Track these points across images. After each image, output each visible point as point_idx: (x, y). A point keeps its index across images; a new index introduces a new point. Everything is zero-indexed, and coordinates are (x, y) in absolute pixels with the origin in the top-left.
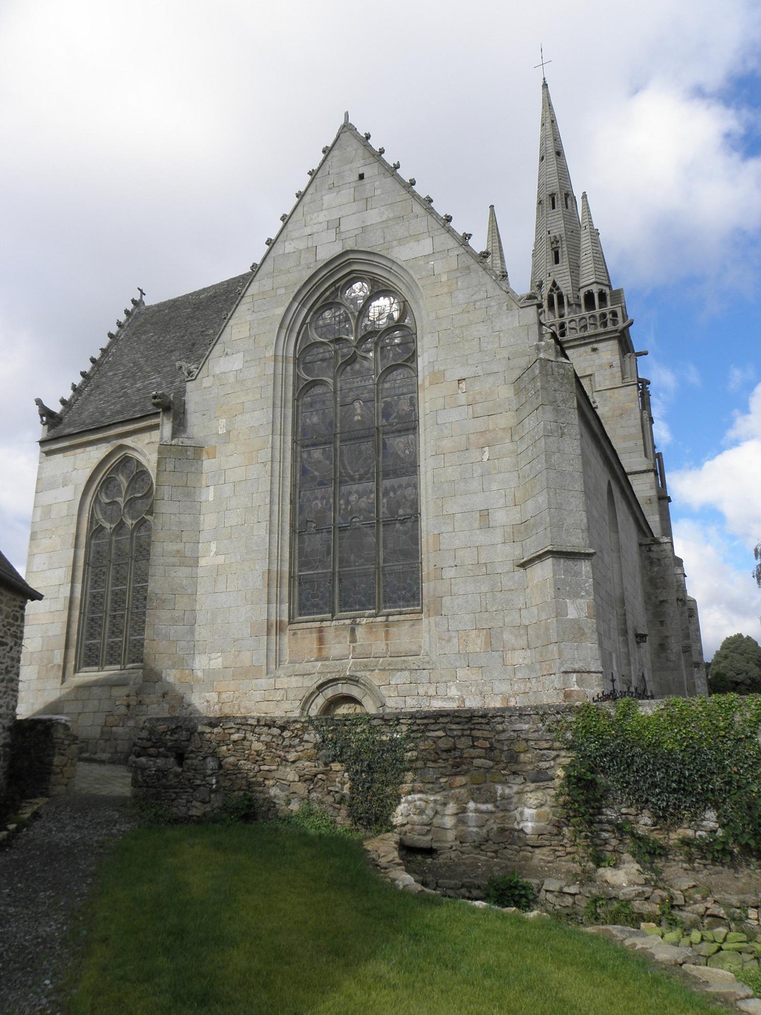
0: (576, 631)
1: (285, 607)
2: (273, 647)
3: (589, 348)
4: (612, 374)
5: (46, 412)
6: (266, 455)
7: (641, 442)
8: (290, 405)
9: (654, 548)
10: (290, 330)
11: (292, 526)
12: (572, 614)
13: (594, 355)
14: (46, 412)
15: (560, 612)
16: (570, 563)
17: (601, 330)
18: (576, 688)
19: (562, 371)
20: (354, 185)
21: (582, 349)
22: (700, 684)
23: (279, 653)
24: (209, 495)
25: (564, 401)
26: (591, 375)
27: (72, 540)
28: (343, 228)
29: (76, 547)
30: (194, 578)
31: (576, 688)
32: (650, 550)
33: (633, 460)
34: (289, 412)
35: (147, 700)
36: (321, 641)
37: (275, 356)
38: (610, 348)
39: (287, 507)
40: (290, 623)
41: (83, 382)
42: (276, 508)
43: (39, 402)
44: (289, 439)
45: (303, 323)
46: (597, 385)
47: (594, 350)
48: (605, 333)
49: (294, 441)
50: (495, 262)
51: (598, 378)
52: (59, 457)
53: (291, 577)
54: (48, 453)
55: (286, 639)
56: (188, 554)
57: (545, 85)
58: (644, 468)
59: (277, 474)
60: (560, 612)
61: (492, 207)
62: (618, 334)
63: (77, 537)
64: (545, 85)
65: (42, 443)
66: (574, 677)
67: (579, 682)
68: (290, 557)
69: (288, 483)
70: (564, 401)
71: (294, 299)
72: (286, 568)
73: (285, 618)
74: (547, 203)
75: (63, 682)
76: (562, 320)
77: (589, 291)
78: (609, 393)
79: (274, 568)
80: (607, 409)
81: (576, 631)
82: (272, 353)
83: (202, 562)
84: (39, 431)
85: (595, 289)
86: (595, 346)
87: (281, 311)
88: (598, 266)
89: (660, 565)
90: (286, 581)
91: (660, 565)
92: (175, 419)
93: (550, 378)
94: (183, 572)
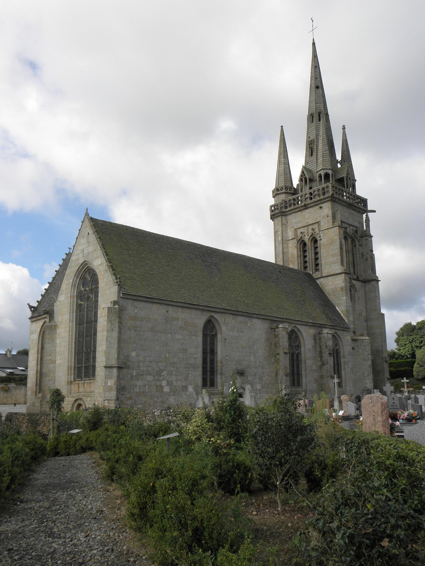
0: (110, 389)
1: (73, 376)
2: (69, 389)
3: (318, 207)
4: (328, 221)
5: (31, 307)
6: (68, 330)
7: (339, 257)
8: (75, 312)
9: (276, 330)
10: (75, 286)
11: (75, 351)
12: (109, 384)
13: (321, 211)
14: (31, 307)
15: (106, 383)
16: (110, 369)
17: (322, 197)
18: (107, 404)
19: (115, 310)
20: (87, 237)
21: (316, 208)
22: (368, 382)
23: (71, 390)
24: (58, 341)
25: (114, 320)
26: (319, 222)
27: (36, 351)
28: (84, 253)
29: (38, 353)
30: (55, 367)
31: (107, 404)
32: (275, 331)
33: (336, 267)
34: (75, 314)
35: (43, 404)
36: (79, 387)
37: (71, 296)
38: (327, 206)
39: (74, 345)
40: (74, 381)
41: (45, 292)
42: (70, 346)
43: (28, 304)
44: (74, 323)
45: (78, 284)
46: (322, 227)
47: (321, 208)
48: (324, 199)
49: (76, 324)
50: (281, 160)
51: (322, 224)
52: (34, 323)
53: (75, 367)
54: (32, 322)
55: (73, 386)
56: (53, 360)
57: (314, 44)
58: (340, 271)
59: (71, 335)
60: (106, 383)
61: (282, 126)
62: (330, 199)
63: (38, 351)
64: (314, 44)
65: (30, 318)
66: (107, 401)
67: (108, 403)
68: (74, 361)
69: (74, 338)
70: (114, 320)
71: (75, 276)
72: (73, 365)
73: (73, 380)
74: (316, 118)
75: (36, 396)
76: (312, 191)
77: (327, 173)
78: (326, 231)
79: (70, 365)
80: (325, 240)
81: (110, 389)
82: (69, 295)
83: (57, 362)
84: (29, 314)
85: (322, 173)
86: (321, 205)
87: (72, 281)
88: (325, 159)
89: (278, 338)
90: (73, 368)
91: (278, 338)
92: (50, 316)
93: (110, 314)
94: (52, 365)
